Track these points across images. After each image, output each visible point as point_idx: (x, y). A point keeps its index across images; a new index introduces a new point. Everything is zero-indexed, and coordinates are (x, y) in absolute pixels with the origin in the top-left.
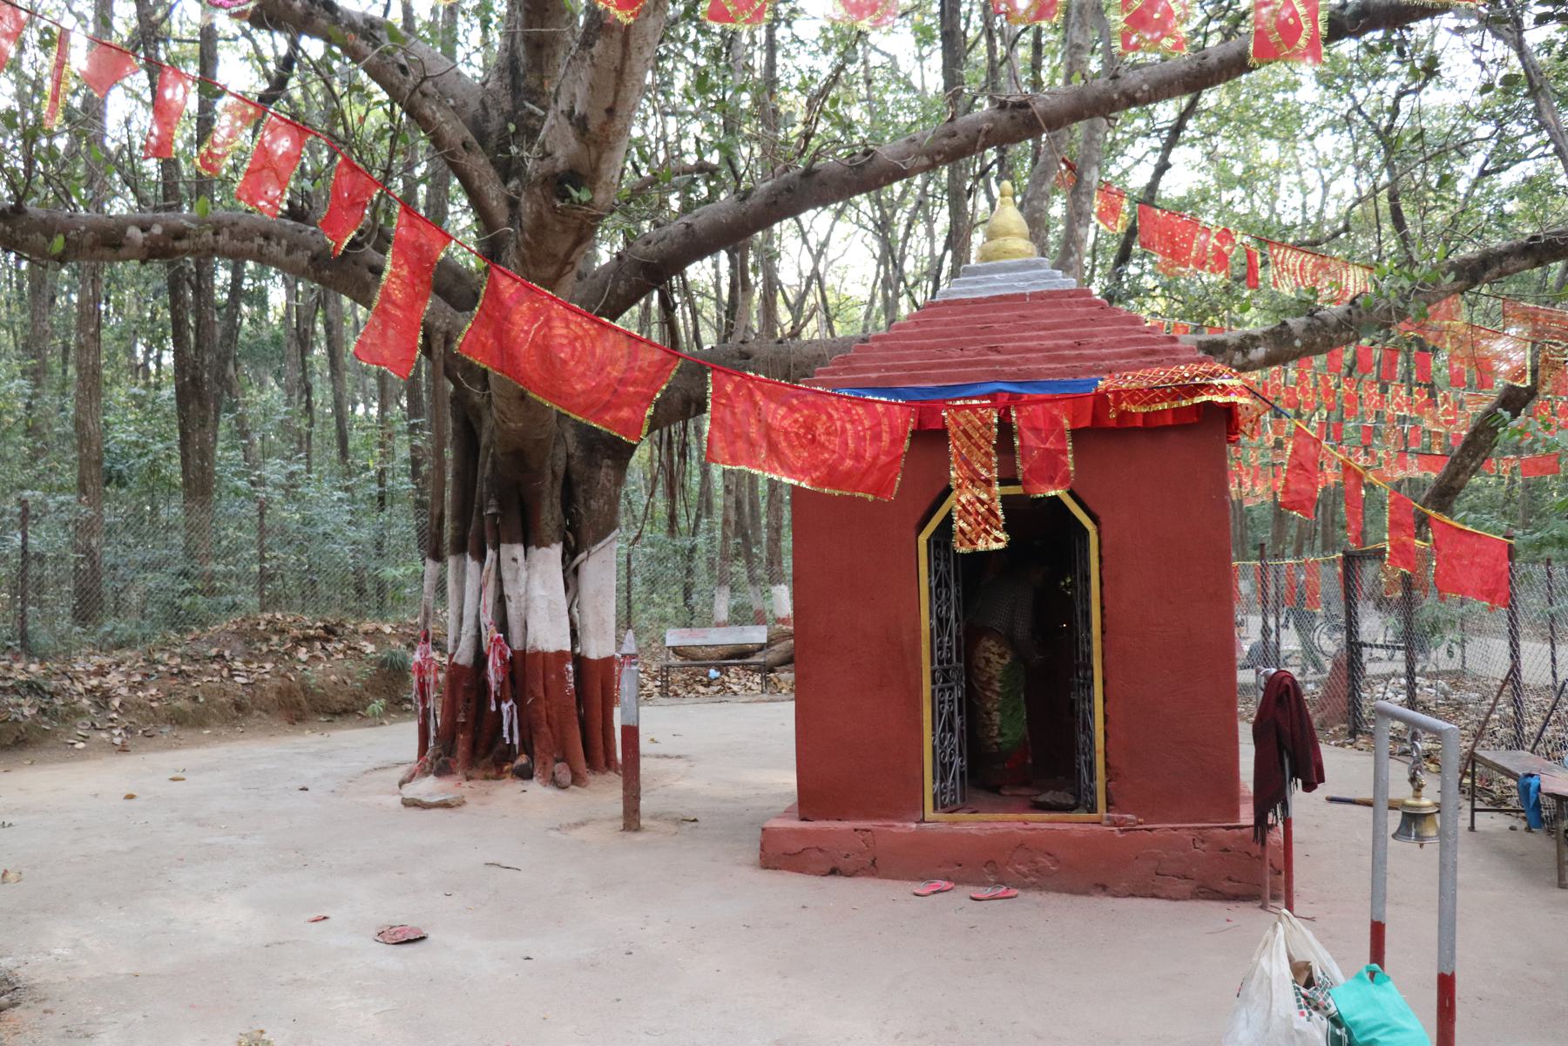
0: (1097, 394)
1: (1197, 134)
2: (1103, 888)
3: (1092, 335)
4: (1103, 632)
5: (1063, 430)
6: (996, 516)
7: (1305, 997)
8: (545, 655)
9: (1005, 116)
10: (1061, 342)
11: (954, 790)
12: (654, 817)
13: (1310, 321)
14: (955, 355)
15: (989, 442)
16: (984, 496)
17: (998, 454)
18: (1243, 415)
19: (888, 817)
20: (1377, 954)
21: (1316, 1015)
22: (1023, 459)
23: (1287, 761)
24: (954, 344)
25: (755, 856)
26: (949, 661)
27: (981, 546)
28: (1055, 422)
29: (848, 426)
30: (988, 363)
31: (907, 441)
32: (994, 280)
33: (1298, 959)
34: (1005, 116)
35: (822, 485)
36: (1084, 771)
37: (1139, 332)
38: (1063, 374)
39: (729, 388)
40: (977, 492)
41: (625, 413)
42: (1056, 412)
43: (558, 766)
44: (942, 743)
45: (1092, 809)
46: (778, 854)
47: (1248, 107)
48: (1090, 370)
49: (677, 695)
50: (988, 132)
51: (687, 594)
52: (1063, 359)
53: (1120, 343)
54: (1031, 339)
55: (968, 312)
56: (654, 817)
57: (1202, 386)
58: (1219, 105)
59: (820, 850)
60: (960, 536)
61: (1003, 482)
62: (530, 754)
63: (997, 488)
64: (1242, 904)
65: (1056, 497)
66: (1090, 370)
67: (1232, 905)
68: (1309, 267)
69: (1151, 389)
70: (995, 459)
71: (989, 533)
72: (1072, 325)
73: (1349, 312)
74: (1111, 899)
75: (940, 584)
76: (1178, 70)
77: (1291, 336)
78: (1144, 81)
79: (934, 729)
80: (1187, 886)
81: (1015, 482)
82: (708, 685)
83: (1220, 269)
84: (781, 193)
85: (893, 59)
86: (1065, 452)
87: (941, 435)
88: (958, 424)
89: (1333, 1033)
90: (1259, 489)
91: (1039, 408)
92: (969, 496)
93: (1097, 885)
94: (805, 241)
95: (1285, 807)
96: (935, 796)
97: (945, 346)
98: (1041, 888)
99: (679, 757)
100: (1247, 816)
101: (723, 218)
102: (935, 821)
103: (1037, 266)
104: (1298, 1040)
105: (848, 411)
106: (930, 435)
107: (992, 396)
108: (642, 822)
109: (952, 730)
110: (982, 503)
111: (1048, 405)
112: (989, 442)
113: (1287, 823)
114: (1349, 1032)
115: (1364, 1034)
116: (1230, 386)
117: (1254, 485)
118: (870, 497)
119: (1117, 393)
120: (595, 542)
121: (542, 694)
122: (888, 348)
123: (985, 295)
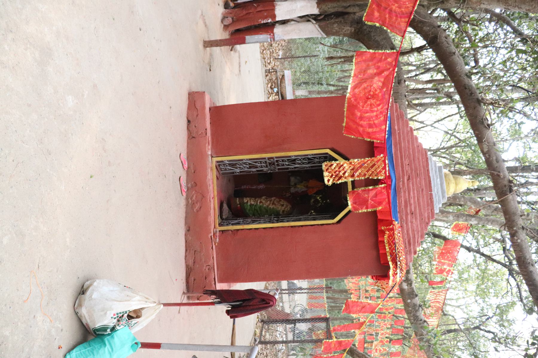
0: (392, 221)
1: (478, 262)
2: (188, 230)
3: (416, 219)
4: (292, 227)
5: (376, 207)
6: (339, 180)
7: (123, 316)
8: (273, 10)
9: (506, 183)
10: (413, 206)
11: (226, 170)
12: (211, 55)
13: (418, 305)
14: (406, 162)
15: (370, 176)
16: (347, 174)
17: (365, 179)
18: (384, 282)
19: (213, 142)
20: (145, 345)
21: (115, 321)
22: (363, 191)
23: (238, 303)
24: (410, 161)
25: (195, 90)
26: (278, 165)
27: (326, 174)
28: (380, 204)
29: (375, 114)
30: (403, 175)
31: (369, 140)
32: (437, 179)
33: (143, 312)
34: (506, 183)
35: (348, 103)
36: (236, 221)
37: (418, 238)
38: (400, 207)
39: (389, 60)
40: (349, 171)
41: (376, 14)
42: (384, 203)
43: (230, 19)
44: (245, 163)
45: (220, 225)
46: (194, 99)
47: (488, 280)
48: (402, 218)
49: (266, 76)
50: (499, 176)
51: (306, 83)
52: (406, 206)
53: (413, 231)
54: (414, 194)
55: (424, 168)
56: (211, 55)
57: (396, 265)
58: (489, 270)
59: (197, 116)
60: (329, 164)
61: (353, 182)
62: (235, 7)
63: (351, 179)
64: (185, 284)
65: (347, 205)
66: (402, 218)
67: (184, 281)
68: (438, 305)
69: (395, 244)
70: (363, 178)
71: (331, 177)
72: (420, 210)
73: (421, 320)
74: (184, 233)
75: (310, 159)
76: (527, 254)
77: (412, 298)
78: (522, 240)
79: (250, 159)
80: (191, 263)
81: (353, 187)
82: (271, 88)
83: (437, 271)
84: (470, 90)
85: (506, 151)
86: (367, 208)
87: (372, 154)
88: (378, 161)
89: (108, 328)
90: (350, 284)
91: (386, 197)
92: (347, 168)
93: (189, 227)
94: (435, 122)
95: (219, 303)
96: (222, 161)
97: (409, 158)
98: (187, 205)
99: (240, 71)
100: (220, 286)
101: (458, 68)
102: (211, 162)
103: (443, 197)
104: (102, 313)
105: (381, 113)
106: (371, 150)
107: (389, 177)
108: (208, 49)
109: (250, 167)
110: (344, 174)
111: (387, 200)
112: (370, 176)
113: (213, 304)
114: (109, 335)
115: (109, 341)
116: (396, 277)
117: (353, 283)
118: (344, 124)
119: (393, 229)
120: (320, 27)
121: (259, 9)
122: (408, 134)
123: (431, 175)
